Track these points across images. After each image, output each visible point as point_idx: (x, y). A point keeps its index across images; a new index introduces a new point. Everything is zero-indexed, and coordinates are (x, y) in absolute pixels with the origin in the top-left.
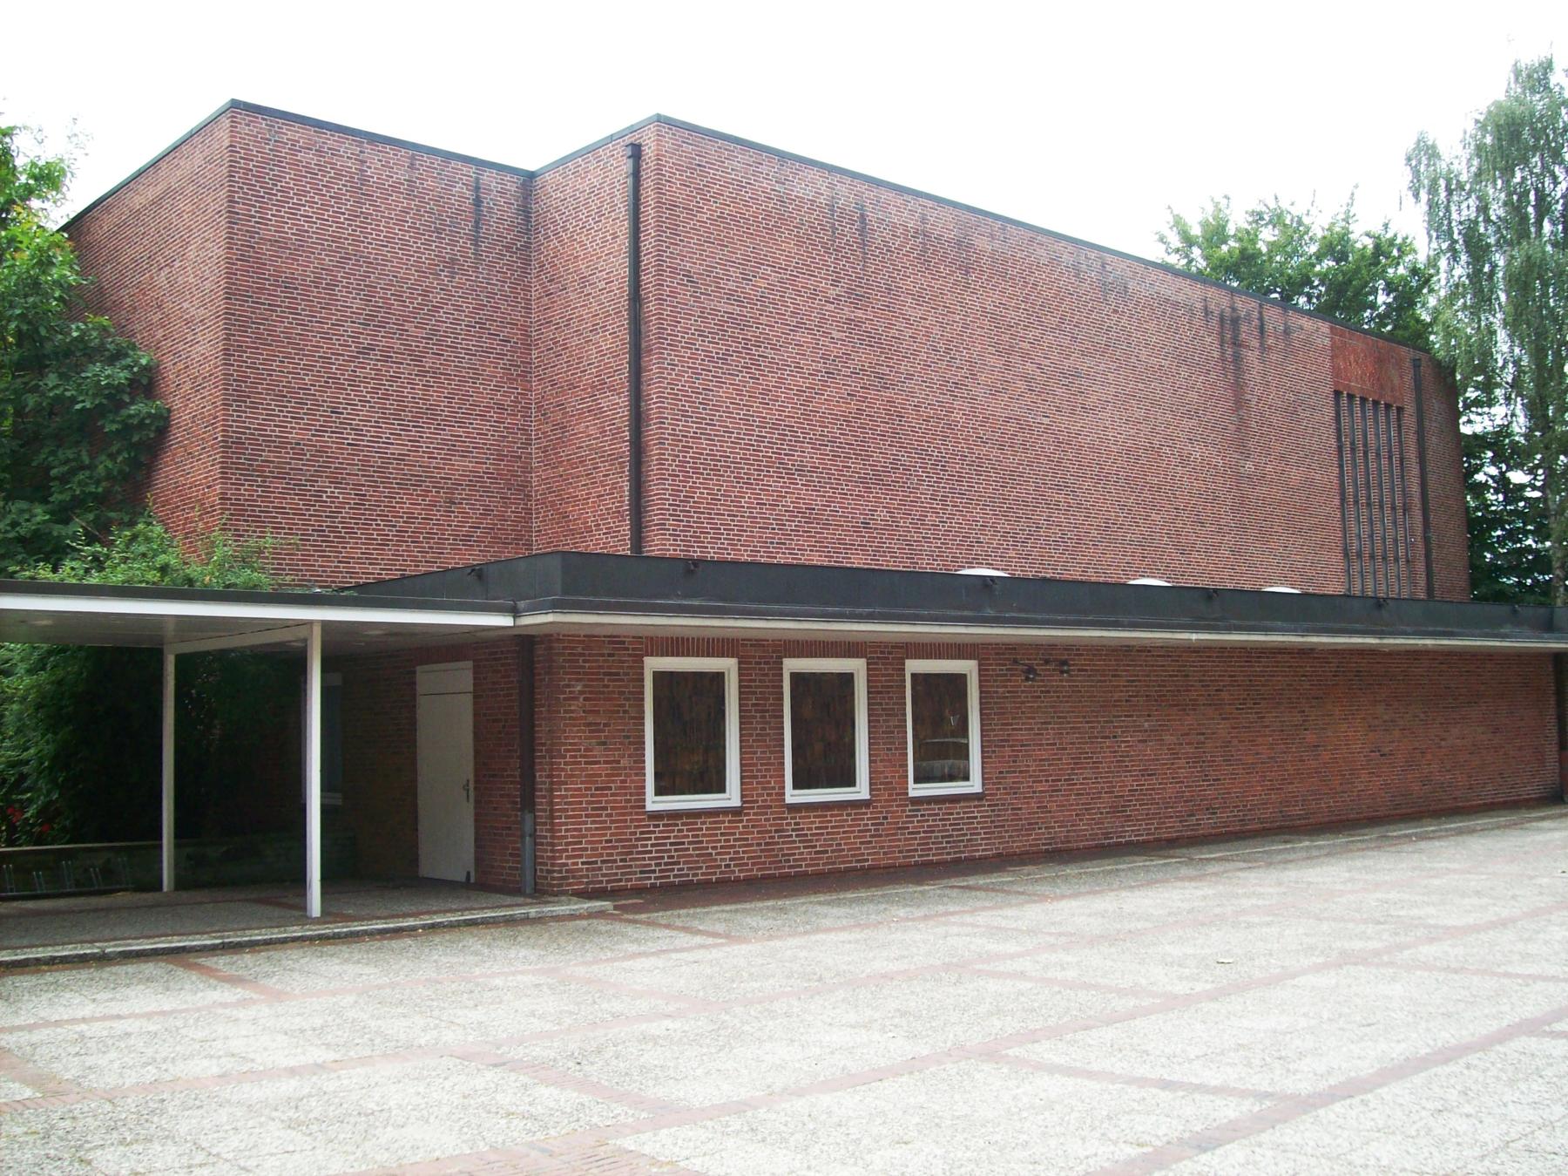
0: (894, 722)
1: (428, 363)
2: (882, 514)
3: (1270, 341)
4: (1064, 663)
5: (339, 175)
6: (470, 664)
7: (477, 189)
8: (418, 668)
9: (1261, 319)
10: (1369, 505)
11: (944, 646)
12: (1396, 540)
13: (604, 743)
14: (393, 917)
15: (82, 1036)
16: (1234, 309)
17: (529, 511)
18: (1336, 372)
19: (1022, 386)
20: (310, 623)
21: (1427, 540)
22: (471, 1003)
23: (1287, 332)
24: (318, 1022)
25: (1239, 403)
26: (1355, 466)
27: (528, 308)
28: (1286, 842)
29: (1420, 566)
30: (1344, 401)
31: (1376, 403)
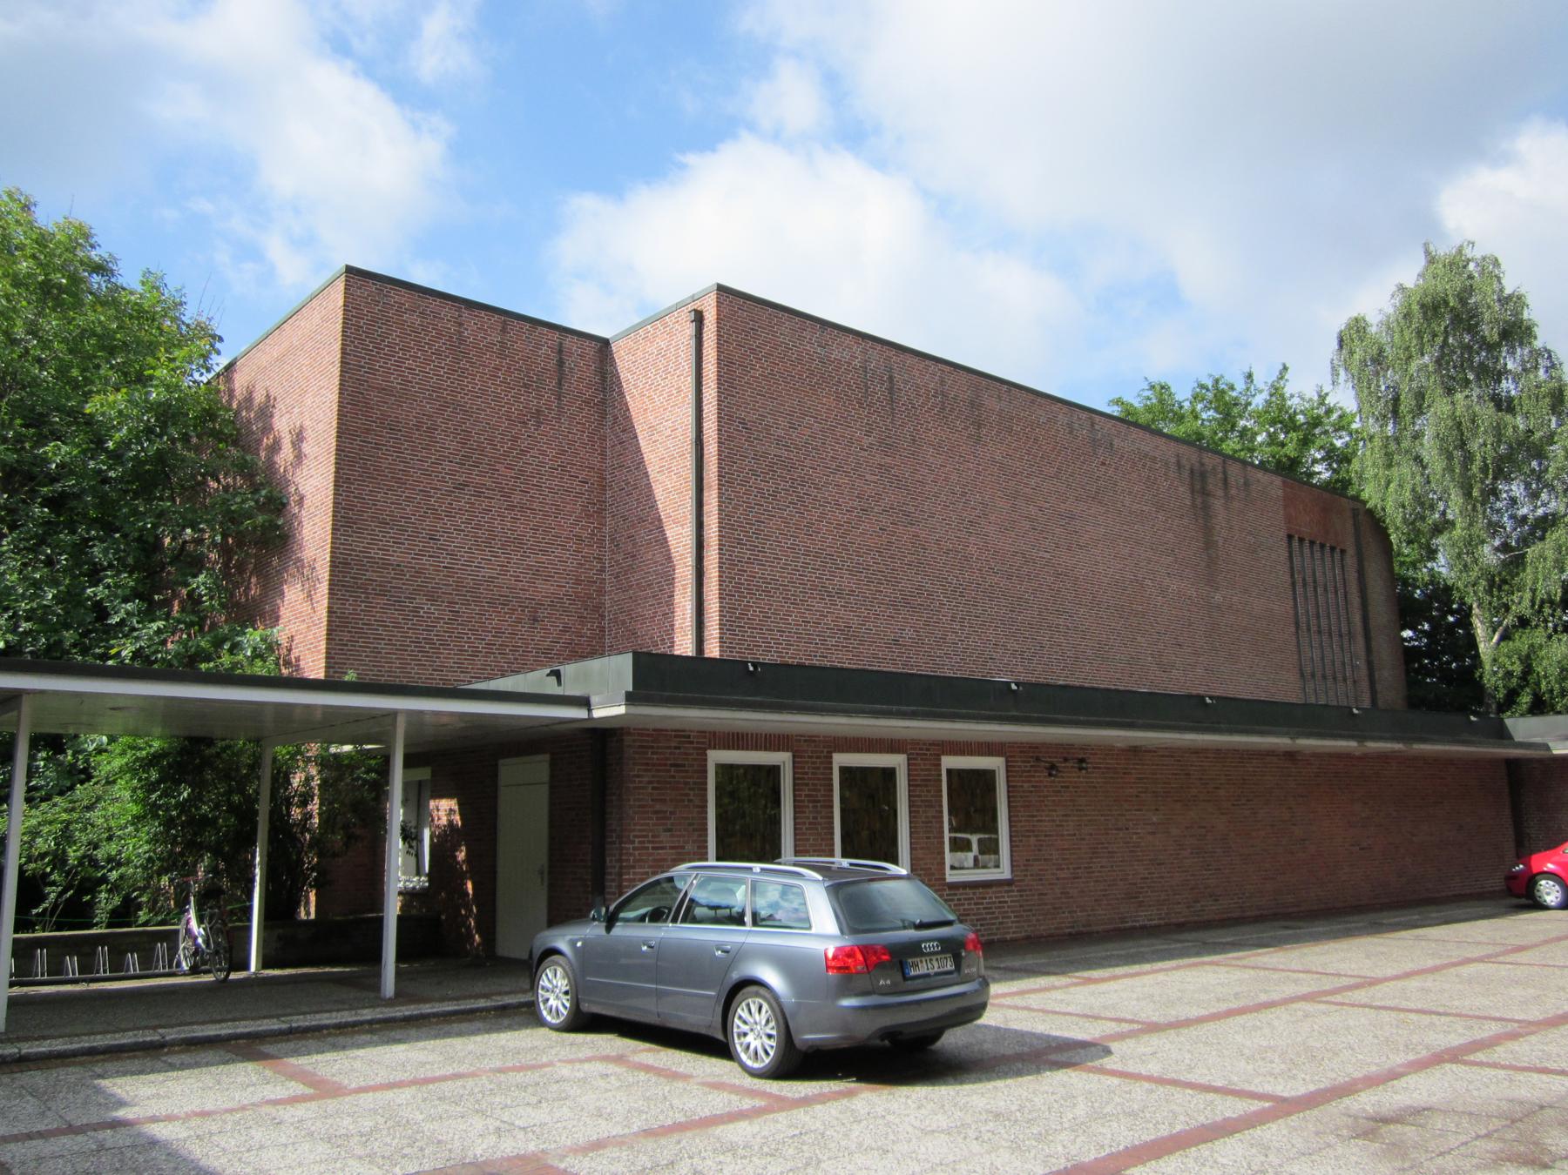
0: (931, 812)
1: (516, 499)
2: (909, 633)
3: (1233, 492)
4: (1082, 761)
5: (439, 335)
6: (547, 757)
7: (560, 352)
8: (501, 762)
9: (1225, 473)
10: (1320, 632)
11: (976, 745)
12: (1343, 664)
13: (670, 830)
14: (465, 998)
15: (101, 1148)
16: (1202, 464)
17: (602, 629)
18: (1289, 519)
19: (1026, 524)
20: (392, 714)
21: (1370, 664)
22: (534, 1100)
23: (1246, 484)
24: (367, 1124)
25: (1209, 545)
26: (1306, 599)
27: (603, 455)
28: (1287, 928)
29: (1365, 685)
30: (1295, 543)
31: (1322, 546)
